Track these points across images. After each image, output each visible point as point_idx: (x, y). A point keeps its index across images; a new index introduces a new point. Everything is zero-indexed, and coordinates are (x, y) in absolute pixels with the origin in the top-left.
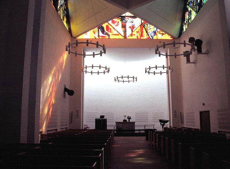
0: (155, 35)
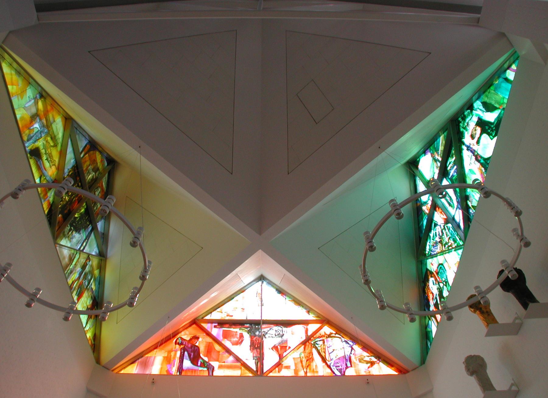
0: (349, 365)
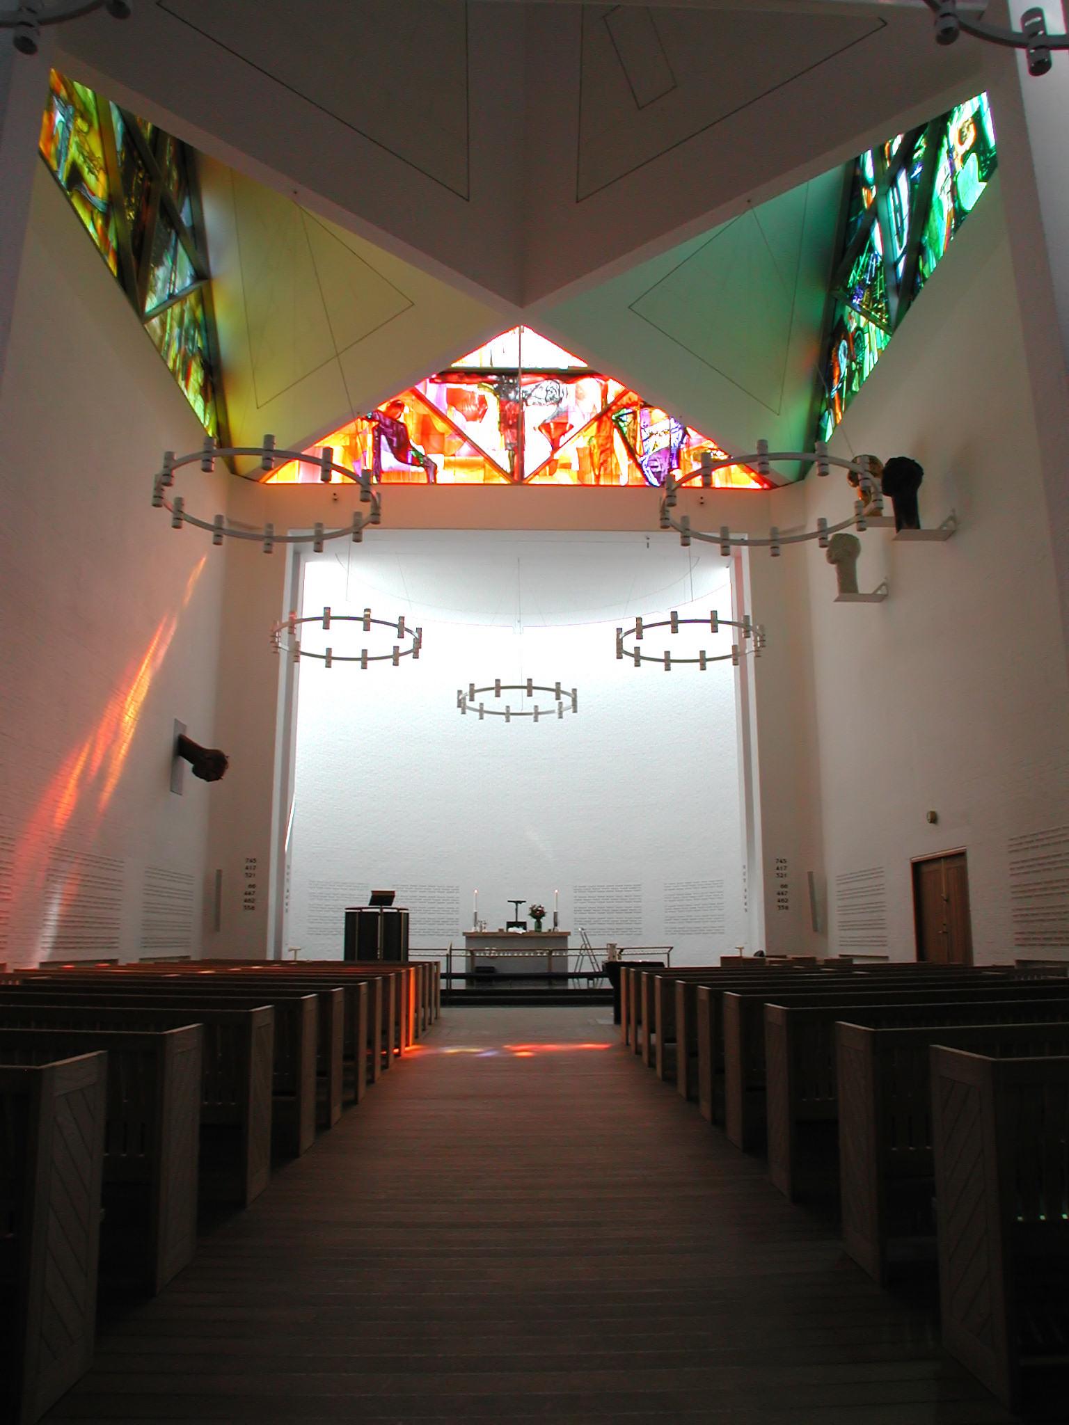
0: (675, 466)
